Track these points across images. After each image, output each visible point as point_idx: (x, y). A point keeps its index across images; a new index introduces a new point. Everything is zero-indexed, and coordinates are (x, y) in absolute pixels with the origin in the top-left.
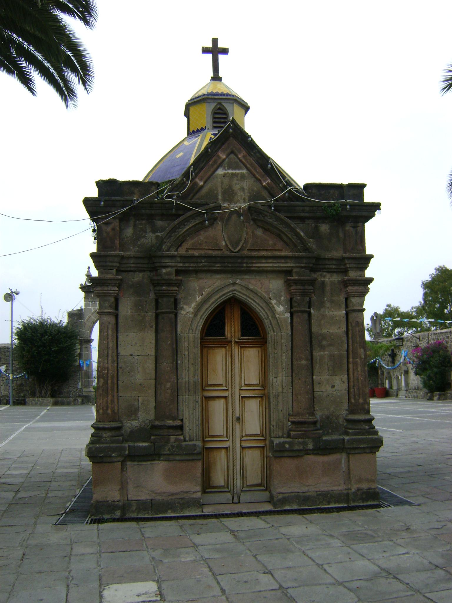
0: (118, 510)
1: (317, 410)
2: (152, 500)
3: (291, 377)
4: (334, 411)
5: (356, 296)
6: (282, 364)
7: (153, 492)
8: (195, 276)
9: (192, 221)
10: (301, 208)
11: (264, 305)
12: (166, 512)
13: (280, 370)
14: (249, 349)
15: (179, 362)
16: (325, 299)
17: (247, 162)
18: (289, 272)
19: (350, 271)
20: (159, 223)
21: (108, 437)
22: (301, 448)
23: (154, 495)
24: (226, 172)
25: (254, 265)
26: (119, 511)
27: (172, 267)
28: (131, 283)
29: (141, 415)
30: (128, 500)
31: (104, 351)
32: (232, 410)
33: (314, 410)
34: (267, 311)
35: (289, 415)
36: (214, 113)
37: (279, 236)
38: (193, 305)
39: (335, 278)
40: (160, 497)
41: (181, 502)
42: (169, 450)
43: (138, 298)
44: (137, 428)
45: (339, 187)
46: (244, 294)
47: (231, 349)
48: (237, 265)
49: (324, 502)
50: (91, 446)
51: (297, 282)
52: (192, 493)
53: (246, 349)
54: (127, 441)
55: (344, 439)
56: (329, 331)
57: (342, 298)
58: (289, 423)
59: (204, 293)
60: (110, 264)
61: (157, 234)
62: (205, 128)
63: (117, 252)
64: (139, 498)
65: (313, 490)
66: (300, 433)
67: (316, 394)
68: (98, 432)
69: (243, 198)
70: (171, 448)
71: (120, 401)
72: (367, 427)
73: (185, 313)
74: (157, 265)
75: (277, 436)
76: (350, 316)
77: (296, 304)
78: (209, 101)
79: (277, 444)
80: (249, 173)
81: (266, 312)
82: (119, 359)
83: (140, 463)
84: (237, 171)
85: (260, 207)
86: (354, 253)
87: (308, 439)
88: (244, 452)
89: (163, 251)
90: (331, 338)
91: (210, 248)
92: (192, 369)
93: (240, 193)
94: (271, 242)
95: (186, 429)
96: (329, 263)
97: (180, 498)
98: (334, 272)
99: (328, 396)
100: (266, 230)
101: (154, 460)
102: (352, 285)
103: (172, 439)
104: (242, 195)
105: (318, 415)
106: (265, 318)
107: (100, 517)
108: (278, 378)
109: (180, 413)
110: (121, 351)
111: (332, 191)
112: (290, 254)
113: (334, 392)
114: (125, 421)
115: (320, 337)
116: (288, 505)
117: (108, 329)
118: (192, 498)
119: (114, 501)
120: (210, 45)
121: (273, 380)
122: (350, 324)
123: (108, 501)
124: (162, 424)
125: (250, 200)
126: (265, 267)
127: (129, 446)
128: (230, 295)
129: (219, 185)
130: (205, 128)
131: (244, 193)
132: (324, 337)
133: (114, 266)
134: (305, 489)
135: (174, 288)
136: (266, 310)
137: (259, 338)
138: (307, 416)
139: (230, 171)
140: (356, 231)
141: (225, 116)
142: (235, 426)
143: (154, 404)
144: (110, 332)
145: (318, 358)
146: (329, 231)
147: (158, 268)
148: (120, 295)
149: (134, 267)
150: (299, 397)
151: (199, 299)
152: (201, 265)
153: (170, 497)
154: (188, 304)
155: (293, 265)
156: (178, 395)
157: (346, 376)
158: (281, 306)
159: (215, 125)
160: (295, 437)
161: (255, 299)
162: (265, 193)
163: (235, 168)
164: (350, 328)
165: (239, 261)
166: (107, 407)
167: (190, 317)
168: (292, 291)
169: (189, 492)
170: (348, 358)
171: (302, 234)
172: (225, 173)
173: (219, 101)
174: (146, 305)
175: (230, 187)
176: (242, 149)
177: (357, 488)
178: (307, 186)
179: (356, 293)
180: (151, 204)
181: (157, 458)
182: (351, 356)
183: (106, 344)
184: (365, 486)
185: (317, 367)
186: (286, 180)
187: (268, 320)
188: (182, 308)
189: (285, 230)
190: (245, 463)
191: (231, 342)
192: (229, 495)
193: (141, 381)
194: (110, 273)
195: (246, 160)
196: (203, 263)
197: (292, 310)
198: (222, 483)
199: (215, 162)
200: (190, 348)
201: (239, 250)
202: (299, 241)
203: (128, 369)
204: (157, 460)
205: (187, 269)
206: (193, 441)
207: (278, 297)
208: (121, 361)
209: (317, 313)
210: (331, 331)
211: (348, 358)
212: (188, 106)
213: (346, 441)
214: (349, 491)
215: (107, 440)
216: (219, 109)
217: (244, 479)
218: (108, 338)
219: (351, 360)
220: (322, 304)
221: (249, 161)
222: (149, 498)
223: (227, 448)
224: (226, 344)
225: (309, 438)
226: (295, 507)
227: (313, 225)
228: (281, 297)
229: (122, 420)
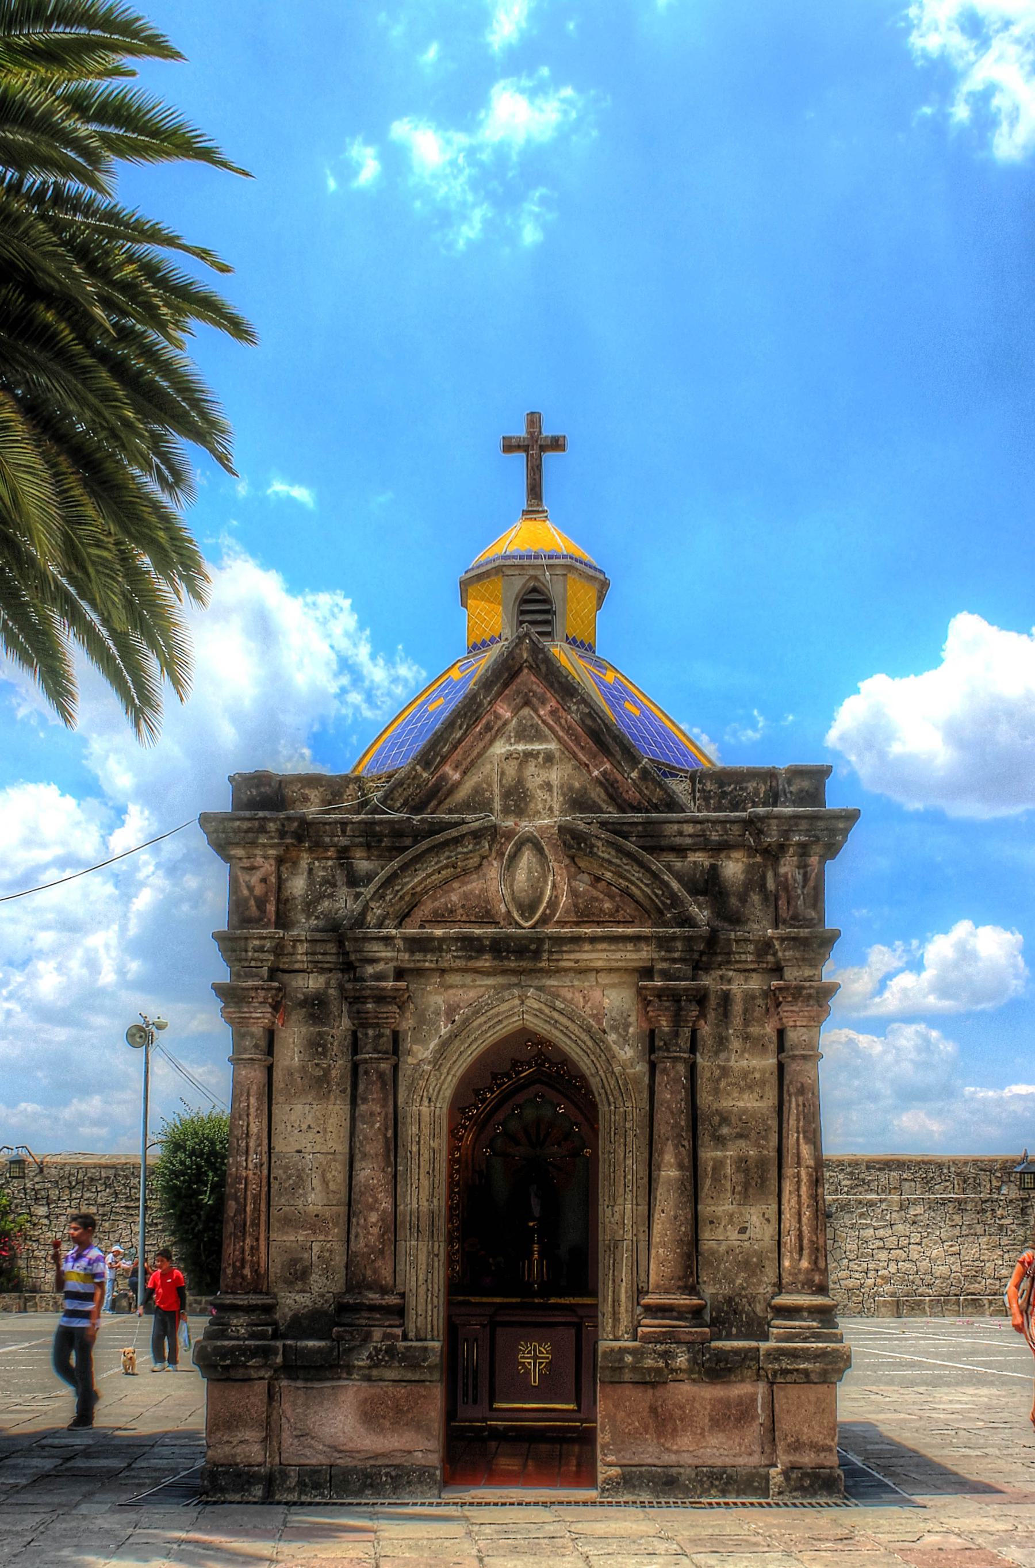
1: (705, 1282)
2: (331, 1466)
3: (646, 1207)
6: (625, 1177)
7: (335, 1448)
10: (676, 827)
13: (621, 1190)
15: (400, 1168)
16: (731, 1031)
24: (512, 748)
25: (566, 956)
27: (387, 961)
29: (317, 1281)
30: (281, 1464)
33: (698, 1283)
38: (433, 1044)
39: (755, 984)
42: (370, 1357)
44: (306, 1309)
50: (204, 1343)
54: (284, 1337)
55: (758, 1349)
59: (457, 1018)
61: (358, 890)
64: (307, 1462)
68: (223, 1315)
71: (272, 1250)
73: (415, 1062)
83: (309, 1385)
84: (537, 747)
89: (368, 928)
90: (740, 1120)
91: (473, 919)
97: (391, 1466)
99: (730, 1250)
103: (377, 1334)
104: (546, 800)
105: (709, 1290)
106: (592, 1075)
108: (616, 1209)
110: (279, 1146)
112: (647, 931)
117: (248, 1096)
119: (250, 1465)
123: (237, 1465)
126: (591, 960)
129: (496, 778)
131: (551, 796)
132: (725, 1120)
133: (262, 961)
139: (521, 747)
141: (548, 607)
144: (252, 1100)
145: (711, 1163)
148: (278, 1023)
154: (424, 1042)
155: (655, 956)
156: (396, 1241)
157: (775, 1206)
158: (627, 1048)
163: (531, 740)
173: (532, 572)
175: (520, 782)
176: (549, 695)
183: (245, 1128)
187: (598, 1079)
188: (409, 1052)
193: (320, 1208)
195: (558, 720)
199: (488, 728)
200: (422, 1137)
201: (537, 923)
203: (291, 1182)
204: (347, 1379)
205: (419, 965)
206: (426, 1340)
210: (741, 1104)
212: (465, 585)
213: (761, 1353)
216: (534, 590)
218: (248, 1115)
221: (563, 721)
222: (325, 1461)
225: (678, 1342)
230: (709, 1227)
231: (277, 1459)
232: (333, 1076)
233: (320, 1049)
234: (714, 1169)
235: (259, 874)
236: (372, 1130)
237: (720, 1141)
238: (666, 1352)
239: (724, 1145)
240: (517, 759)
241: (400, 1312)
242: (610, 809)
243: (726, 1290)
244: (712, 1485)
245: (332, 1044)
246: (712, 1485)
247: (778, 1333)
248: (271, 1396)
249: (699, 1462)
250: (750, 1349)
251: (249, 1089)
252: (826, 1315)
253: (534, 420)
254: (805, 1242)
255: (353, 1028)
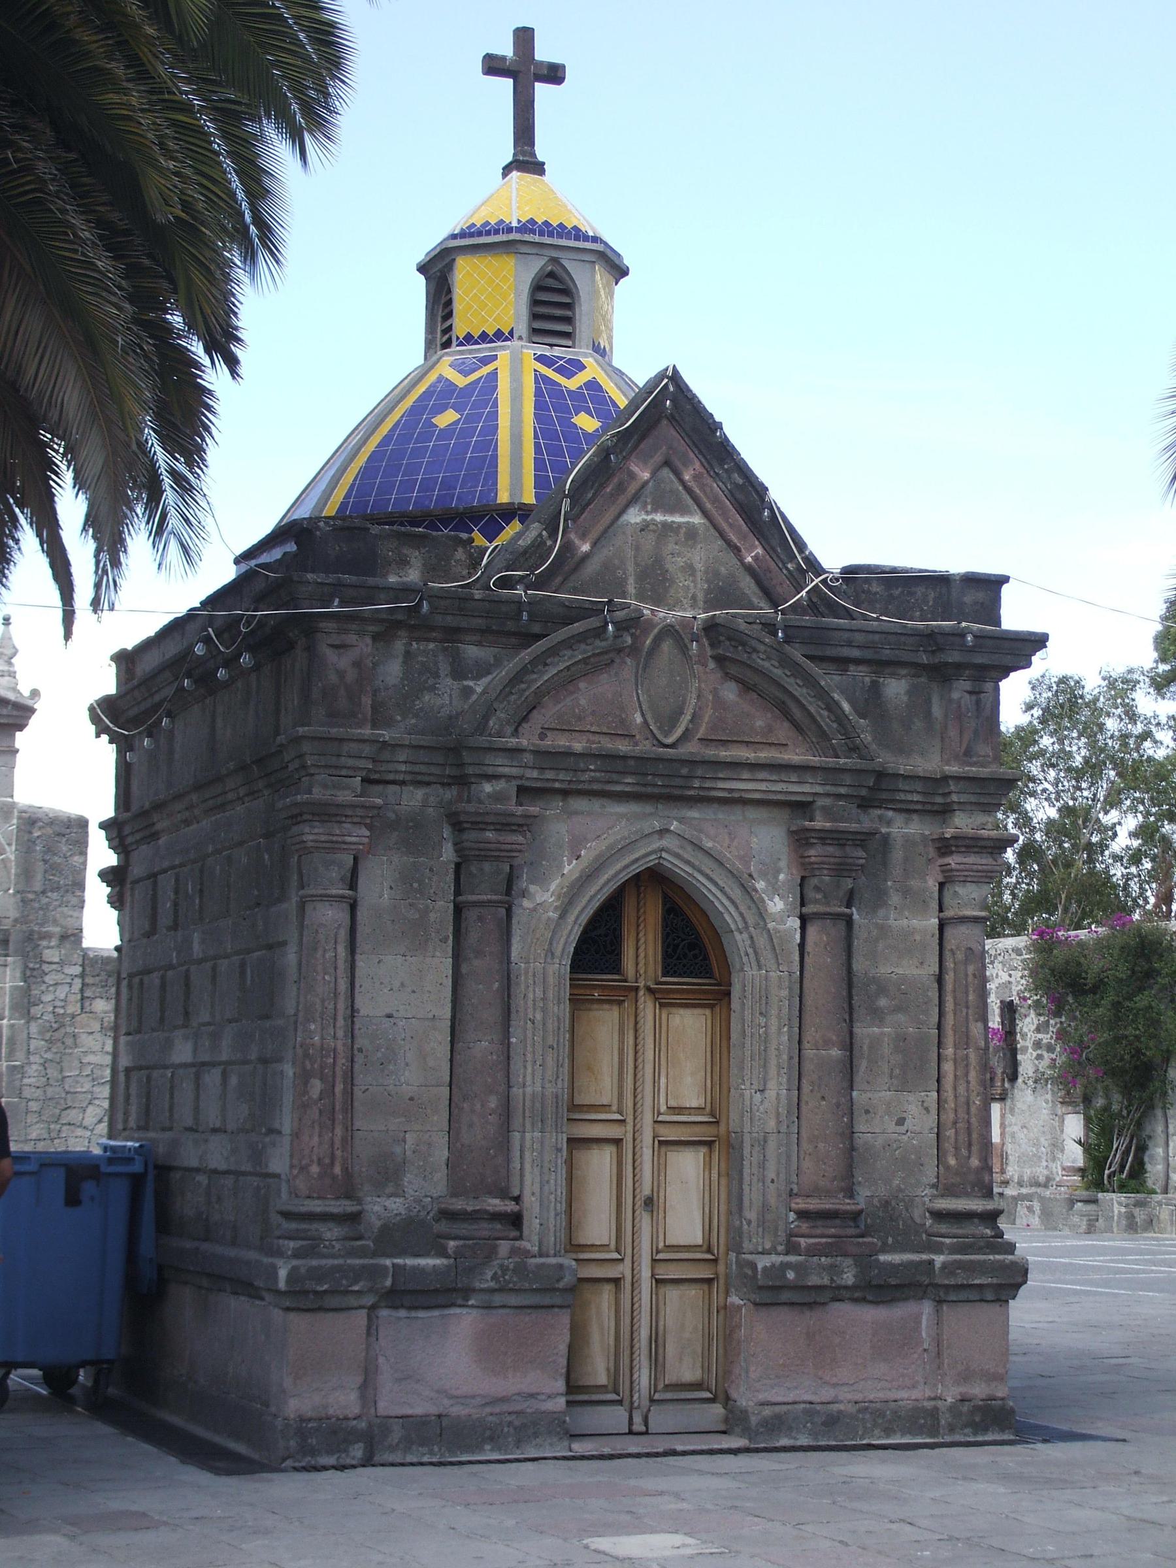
0: (359, 1441)
2: (439, 1416)
4: (902, 1186)
5: (969, 879)
8: (561, 804)
9: (564, 656)
10: (846, 635)
11: (736, 893)
12: (479, 1448)
14: (682, 1011)
17: (705, 493)
18: (802, 807)
19: (957, 813)
20: (472, 652)
21: (337, 1240)
22: (826, 1281)
23: (446, 1402)
24: (649, 518)
25: (721, 785)
26: (361, 1445)
27: (509, 778)
28: (392, 816)
29: (412, 1182)
31: (326, 1004)
32: (634, 1176)
33: (853, 1183)
34: (743, 911)
35: (791, 1194)
36: (538, 287)
37: (783, 707)
40: (462, 1408)
41: (517, 1423)
42: (494, 1277)
43: (412, 860)
44: (398, 1218)
45: (940, 581)
46: (688, 862)
47: (636, 1009)
48: (678, 782)
49: (876, 1432)
51: (825, 837)
52: (543, 1397)
53: (674, 1010)
55: (931, 1263)
56: (896, 970)
57: (932, 884)
58: (792, 1216)
60: (351, 762)
62: (511, 333)
63: (367, 732)
64: (409, 1412)
65: (849, 1396)
66: (824, 1240)
67: (860, 1140)
69: (690, 595)
70: (500, 1272)
72: (988, 1232)
74: (470, 770)
75: (760, 1250)
76: (949, 932)
77: (819, 896)
78: (524, 249)
79: (765, 1268)
80: (708, 524)
81: (741, 914)
82: (357, 1027)
83: (413, 1314)
84: (678, 519)
85: (743, 626)
86: (971, 765)
87: (842, 1258)
88: (661, 1291)
90: (899, 989)
91: (605, 730)
92: (550, 1062)
93: (683, 581)
94: (759, 723)
95: (532, 1224)
96: (907, 788)
98: (915, 811)
100: (746, 687)
101: (453, 1305)
102: (963, 850)
104: (688, 587)
105: (864, 1193)
107: (309, 1461)
109: (515, 1180)
111: (920, 591)
113: (904, 1137)
114: (369, 1199)
115: (874, 987)
116: (786, 1436)
118: (544, 1412)
119: (346, 1418)
120: (506, 49)
121: (751, 1098)
122: (947, 955)
124: (478, 1208)
125: (710, 605)
127: (394, 1265)
128: (651, 861)
129: (630, 553)
130: (511, 333)
132: (882, 990)
133: (354, 769)
134: (826, 1394)
135: (515, 838)
136: (742, 908)
137: (707, 981)
138: (841, 1195)
139: (659, 517)
140: (978, 702)
141: (567, 300)
142: (640, 1221)
143: (446, 1153)
145: (867, 1042)
146: (905, 698)
147: (473, 780)
149: (405, 772)
150: (821, 1145)
151: (571, 868)
152: (586, 776)
153: (488, 1410)
154: (541, 880)
155: (819, 789)
158: (777, 898)
159: (538, 325)
160: (812, 1252)
161: (714, 877)
162: (747, 585)
163: (671, 510)
164: (949, 964)
165: (684, 771)
166: (333, 1157)
167: (549, 918)
168: (813, 859)
169: (538, 1394)
170: (940, 1044)
171: (846, 706)
172: (644, 520)
173: (555, 254)
174: (430, 879)
175: (658, 561)
176: (692, 455)
177: (961, 1394)
178: (851, 573)
179: (972, 874)
180: (461, 600)
181: (460, 1302)
182: (949, 1039)
183: (332, 985)
184: (979, 1390)
185: (862, 1066)
186: (807, 553)
187: (745, 936)
188: (524, 894)
189: (800, 692)
190: (661, 1323)
191: (637, 989)
192: (621, 1413)
194: (347, 787)
195: (702, 487)
196: (591, 774)
197: (805, 910)
198: (602, 1379)
202: (835, 725)
203: (379, 1055)
204: (460, 1306)
206: (548, 1256)
207: (770, 873)
208: (362, 1031)
209: (866, 921)
211: (940, 1044)
214: (939, 1403)
215: (333, 1247)
216: (551, 275)
217: (659, 1368)
218: (336, 968)
219: (949, 1051)
220: (879, 899)
221: (708, 490)
222: (434, 1410)
223: (616, 1281)
224: (622, 995)
225: (845, 1255)
226: (804, 1441)
227: (867, 679)
228: (778, 871)
229: (360, 1194)
230: (864, 1117)
231: (372, 1411)
232: (432, 920)
233: (415, 885)
234: (871, 1047)
235: (352, 654)
236: (481, 992)
237: (878, 1015)
238: (833, 1266)
239: (882, 1020)
240: (654, 531)
241: (516, 1221)
242: (762, 605)
243: (882, 1191)
244: (875, 1425)
245: (430, 879)
246: (875, 1425)
247: (951, 1243)
248: (371, 1330)
249: (859, 1397)
250: (921, 1262)
251: (336, 935)
252: (991, 1217)
253: (524, 37)
254: (975, 1136)
255: (459, 860)
